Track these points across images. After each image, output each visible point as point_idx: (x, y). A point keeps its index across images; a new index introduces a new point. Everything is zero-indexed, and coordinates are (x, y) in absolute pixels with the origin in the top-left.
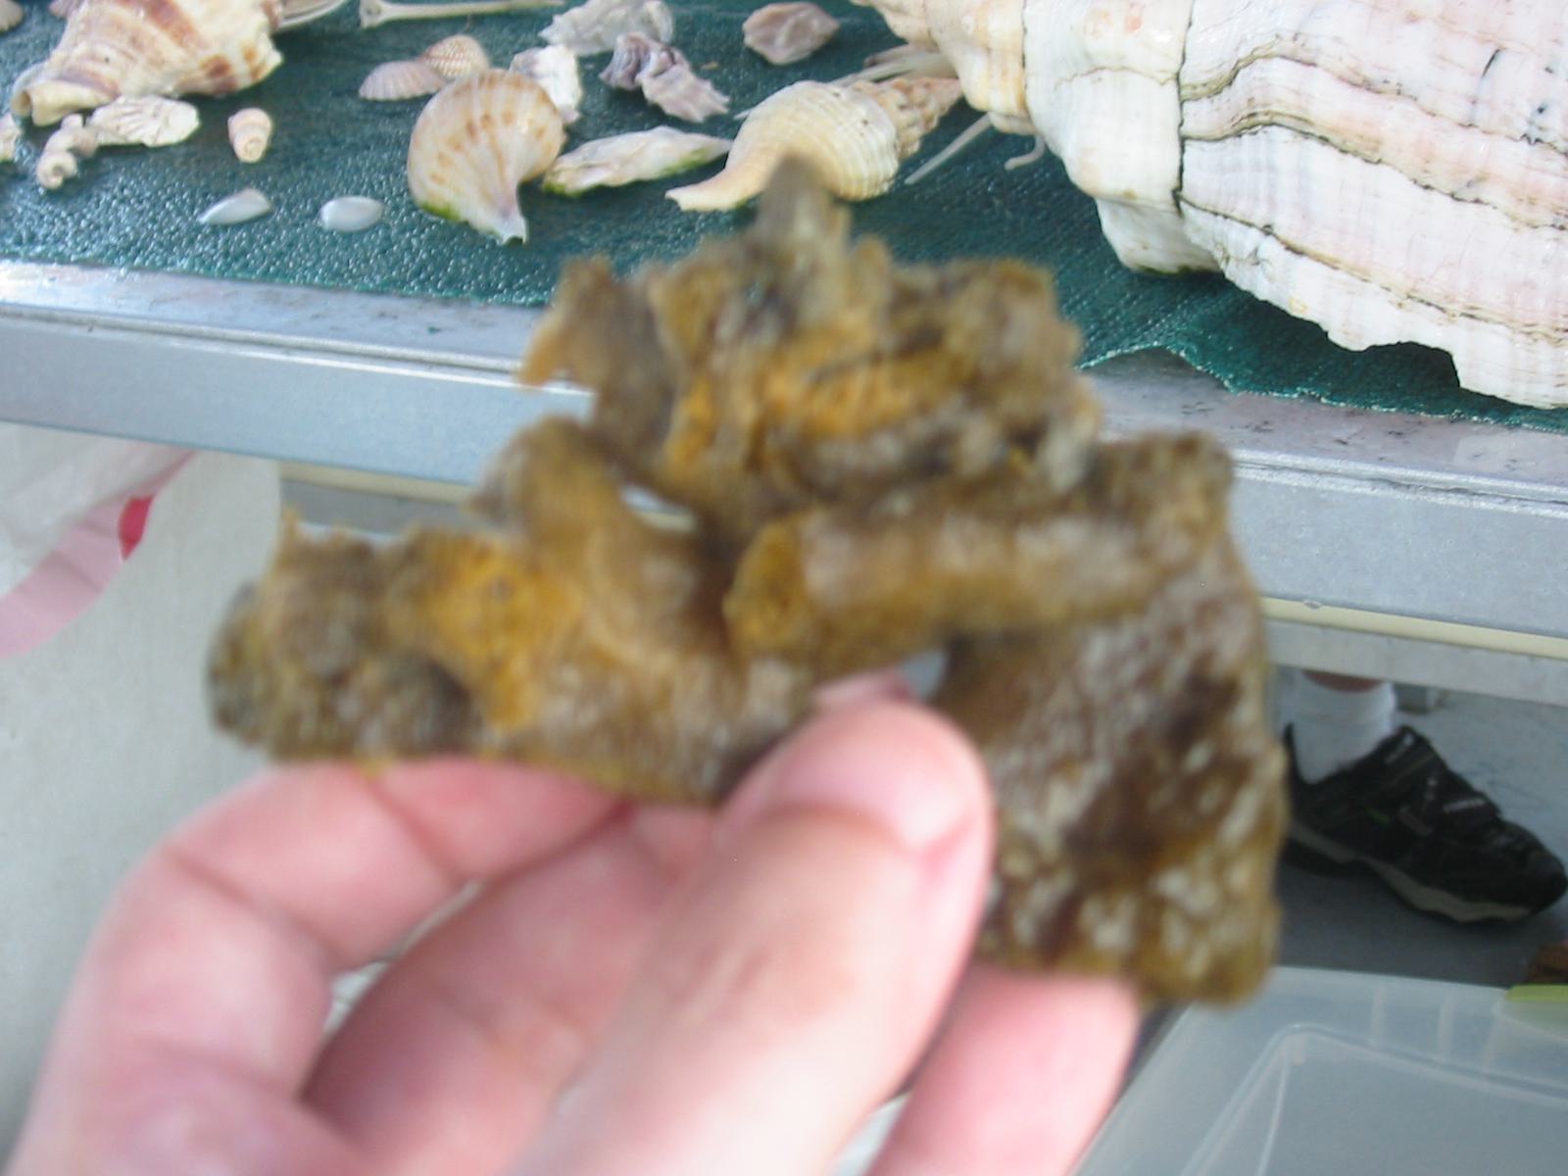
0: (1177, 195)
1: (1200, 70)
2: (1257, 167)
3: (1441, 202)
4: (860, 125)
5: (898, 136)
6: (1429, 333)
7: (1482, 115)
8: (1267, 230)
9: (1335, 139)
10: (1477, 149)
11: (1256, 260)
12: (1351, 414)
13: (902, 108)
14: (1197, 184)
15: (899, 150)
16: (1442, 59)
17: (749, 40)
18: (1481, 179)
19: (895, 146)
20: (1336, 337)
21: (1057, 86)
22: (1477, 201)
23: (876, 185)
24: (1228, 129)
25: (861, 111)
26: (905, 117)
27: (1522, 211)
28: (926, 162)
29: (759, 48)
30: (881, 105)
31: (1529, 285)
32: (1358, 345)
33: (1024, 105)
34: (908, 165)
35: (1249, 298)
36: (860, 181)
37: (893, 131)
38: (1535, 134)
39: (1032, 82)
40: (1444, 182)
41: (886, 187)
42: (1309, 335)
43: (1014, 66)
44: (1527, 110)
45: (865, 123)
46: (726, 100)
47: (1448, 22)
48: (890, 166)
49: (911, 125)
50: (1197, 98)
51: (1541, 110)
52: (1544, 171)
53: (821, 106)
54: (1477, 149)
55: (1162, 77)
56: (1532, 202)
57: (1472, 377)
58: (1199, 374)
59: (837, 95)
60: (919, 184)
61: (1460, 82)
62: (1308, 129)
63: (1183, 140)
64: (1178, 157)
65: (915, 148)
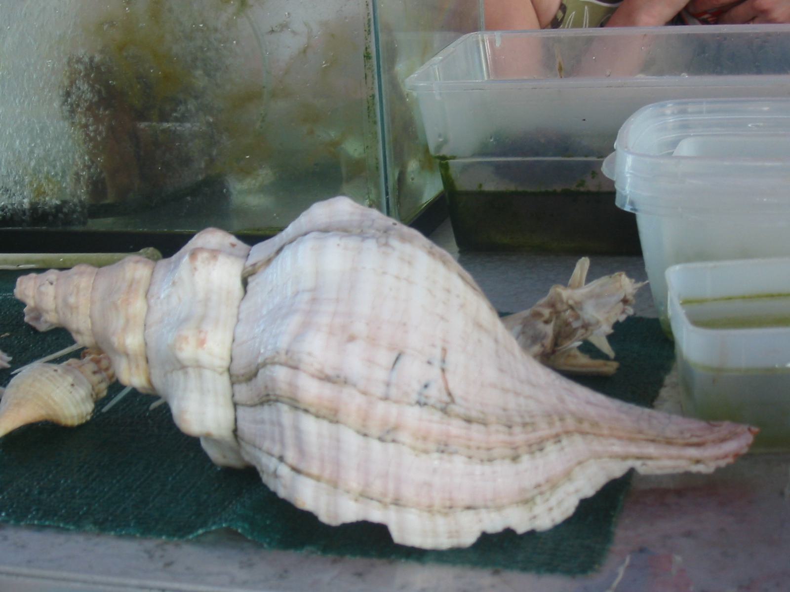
0: (235, 431)
1: (240, 367)
2: (272, 423)
3: (376, 445)
4: (69, 388)
5: (93, 389)
6: (376, 515)
7: (393, 392)
8: (281, 459)
9: (312, 410)
10: (393, 411)
11: (275, 475)
12: (334, 562)
13: (95, 373)
14: (246, 427)
15: (94, 396)
16: (370, 362)
17: (26, 319)
18: (396, 428)
19: (92, 395)
20: (324, 517)
21: (165, 375)
22: (394, 441)
23: (82, 418)
24: (256, 400)
25: (70, 379)
26: (96, 378)
27: (420, 445)
28: (115, 396)
29: (32, 323)
30: (82, 373)
31: (429, 485)
32: (335, 522)
33: (150, 382)
34: (99, 403)
35: (274, 495)
36: (73, 417)
37: (90, 387)
38: (423, 400)
39: (152, 371)
40: (374, 431)
41: (89, 418)
42: (309, 518)
43: (142, 363)
44: (417, 387)
45: (73, 385)
46: (10, 359)
47: (373, 341)
48: (89, 407)
49: (101, 382)
50: (240, 382)
51: (426, 386)
52: (430, 421)
53: (47, 378)
54: (393, 411)
55: (221, 370)
56: (425, 439)
57: (397, 537)
58: (249, 541)
59: (56, 371)
60: (109, 412)
61: (381, 375)
62: (297, 405)
63: (235, 405)
64: (237, 414)
65: (105, 393)
